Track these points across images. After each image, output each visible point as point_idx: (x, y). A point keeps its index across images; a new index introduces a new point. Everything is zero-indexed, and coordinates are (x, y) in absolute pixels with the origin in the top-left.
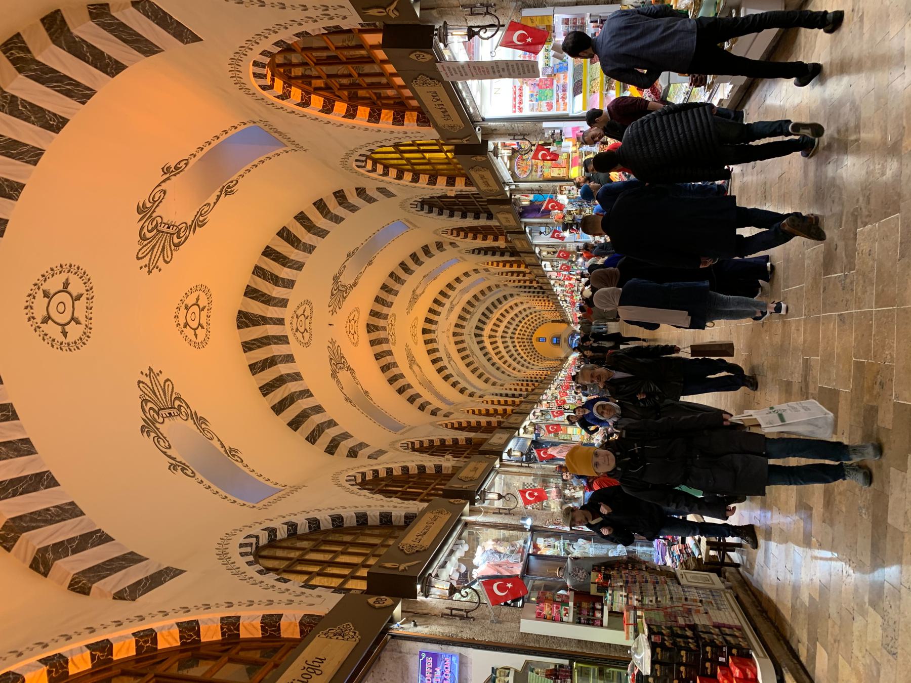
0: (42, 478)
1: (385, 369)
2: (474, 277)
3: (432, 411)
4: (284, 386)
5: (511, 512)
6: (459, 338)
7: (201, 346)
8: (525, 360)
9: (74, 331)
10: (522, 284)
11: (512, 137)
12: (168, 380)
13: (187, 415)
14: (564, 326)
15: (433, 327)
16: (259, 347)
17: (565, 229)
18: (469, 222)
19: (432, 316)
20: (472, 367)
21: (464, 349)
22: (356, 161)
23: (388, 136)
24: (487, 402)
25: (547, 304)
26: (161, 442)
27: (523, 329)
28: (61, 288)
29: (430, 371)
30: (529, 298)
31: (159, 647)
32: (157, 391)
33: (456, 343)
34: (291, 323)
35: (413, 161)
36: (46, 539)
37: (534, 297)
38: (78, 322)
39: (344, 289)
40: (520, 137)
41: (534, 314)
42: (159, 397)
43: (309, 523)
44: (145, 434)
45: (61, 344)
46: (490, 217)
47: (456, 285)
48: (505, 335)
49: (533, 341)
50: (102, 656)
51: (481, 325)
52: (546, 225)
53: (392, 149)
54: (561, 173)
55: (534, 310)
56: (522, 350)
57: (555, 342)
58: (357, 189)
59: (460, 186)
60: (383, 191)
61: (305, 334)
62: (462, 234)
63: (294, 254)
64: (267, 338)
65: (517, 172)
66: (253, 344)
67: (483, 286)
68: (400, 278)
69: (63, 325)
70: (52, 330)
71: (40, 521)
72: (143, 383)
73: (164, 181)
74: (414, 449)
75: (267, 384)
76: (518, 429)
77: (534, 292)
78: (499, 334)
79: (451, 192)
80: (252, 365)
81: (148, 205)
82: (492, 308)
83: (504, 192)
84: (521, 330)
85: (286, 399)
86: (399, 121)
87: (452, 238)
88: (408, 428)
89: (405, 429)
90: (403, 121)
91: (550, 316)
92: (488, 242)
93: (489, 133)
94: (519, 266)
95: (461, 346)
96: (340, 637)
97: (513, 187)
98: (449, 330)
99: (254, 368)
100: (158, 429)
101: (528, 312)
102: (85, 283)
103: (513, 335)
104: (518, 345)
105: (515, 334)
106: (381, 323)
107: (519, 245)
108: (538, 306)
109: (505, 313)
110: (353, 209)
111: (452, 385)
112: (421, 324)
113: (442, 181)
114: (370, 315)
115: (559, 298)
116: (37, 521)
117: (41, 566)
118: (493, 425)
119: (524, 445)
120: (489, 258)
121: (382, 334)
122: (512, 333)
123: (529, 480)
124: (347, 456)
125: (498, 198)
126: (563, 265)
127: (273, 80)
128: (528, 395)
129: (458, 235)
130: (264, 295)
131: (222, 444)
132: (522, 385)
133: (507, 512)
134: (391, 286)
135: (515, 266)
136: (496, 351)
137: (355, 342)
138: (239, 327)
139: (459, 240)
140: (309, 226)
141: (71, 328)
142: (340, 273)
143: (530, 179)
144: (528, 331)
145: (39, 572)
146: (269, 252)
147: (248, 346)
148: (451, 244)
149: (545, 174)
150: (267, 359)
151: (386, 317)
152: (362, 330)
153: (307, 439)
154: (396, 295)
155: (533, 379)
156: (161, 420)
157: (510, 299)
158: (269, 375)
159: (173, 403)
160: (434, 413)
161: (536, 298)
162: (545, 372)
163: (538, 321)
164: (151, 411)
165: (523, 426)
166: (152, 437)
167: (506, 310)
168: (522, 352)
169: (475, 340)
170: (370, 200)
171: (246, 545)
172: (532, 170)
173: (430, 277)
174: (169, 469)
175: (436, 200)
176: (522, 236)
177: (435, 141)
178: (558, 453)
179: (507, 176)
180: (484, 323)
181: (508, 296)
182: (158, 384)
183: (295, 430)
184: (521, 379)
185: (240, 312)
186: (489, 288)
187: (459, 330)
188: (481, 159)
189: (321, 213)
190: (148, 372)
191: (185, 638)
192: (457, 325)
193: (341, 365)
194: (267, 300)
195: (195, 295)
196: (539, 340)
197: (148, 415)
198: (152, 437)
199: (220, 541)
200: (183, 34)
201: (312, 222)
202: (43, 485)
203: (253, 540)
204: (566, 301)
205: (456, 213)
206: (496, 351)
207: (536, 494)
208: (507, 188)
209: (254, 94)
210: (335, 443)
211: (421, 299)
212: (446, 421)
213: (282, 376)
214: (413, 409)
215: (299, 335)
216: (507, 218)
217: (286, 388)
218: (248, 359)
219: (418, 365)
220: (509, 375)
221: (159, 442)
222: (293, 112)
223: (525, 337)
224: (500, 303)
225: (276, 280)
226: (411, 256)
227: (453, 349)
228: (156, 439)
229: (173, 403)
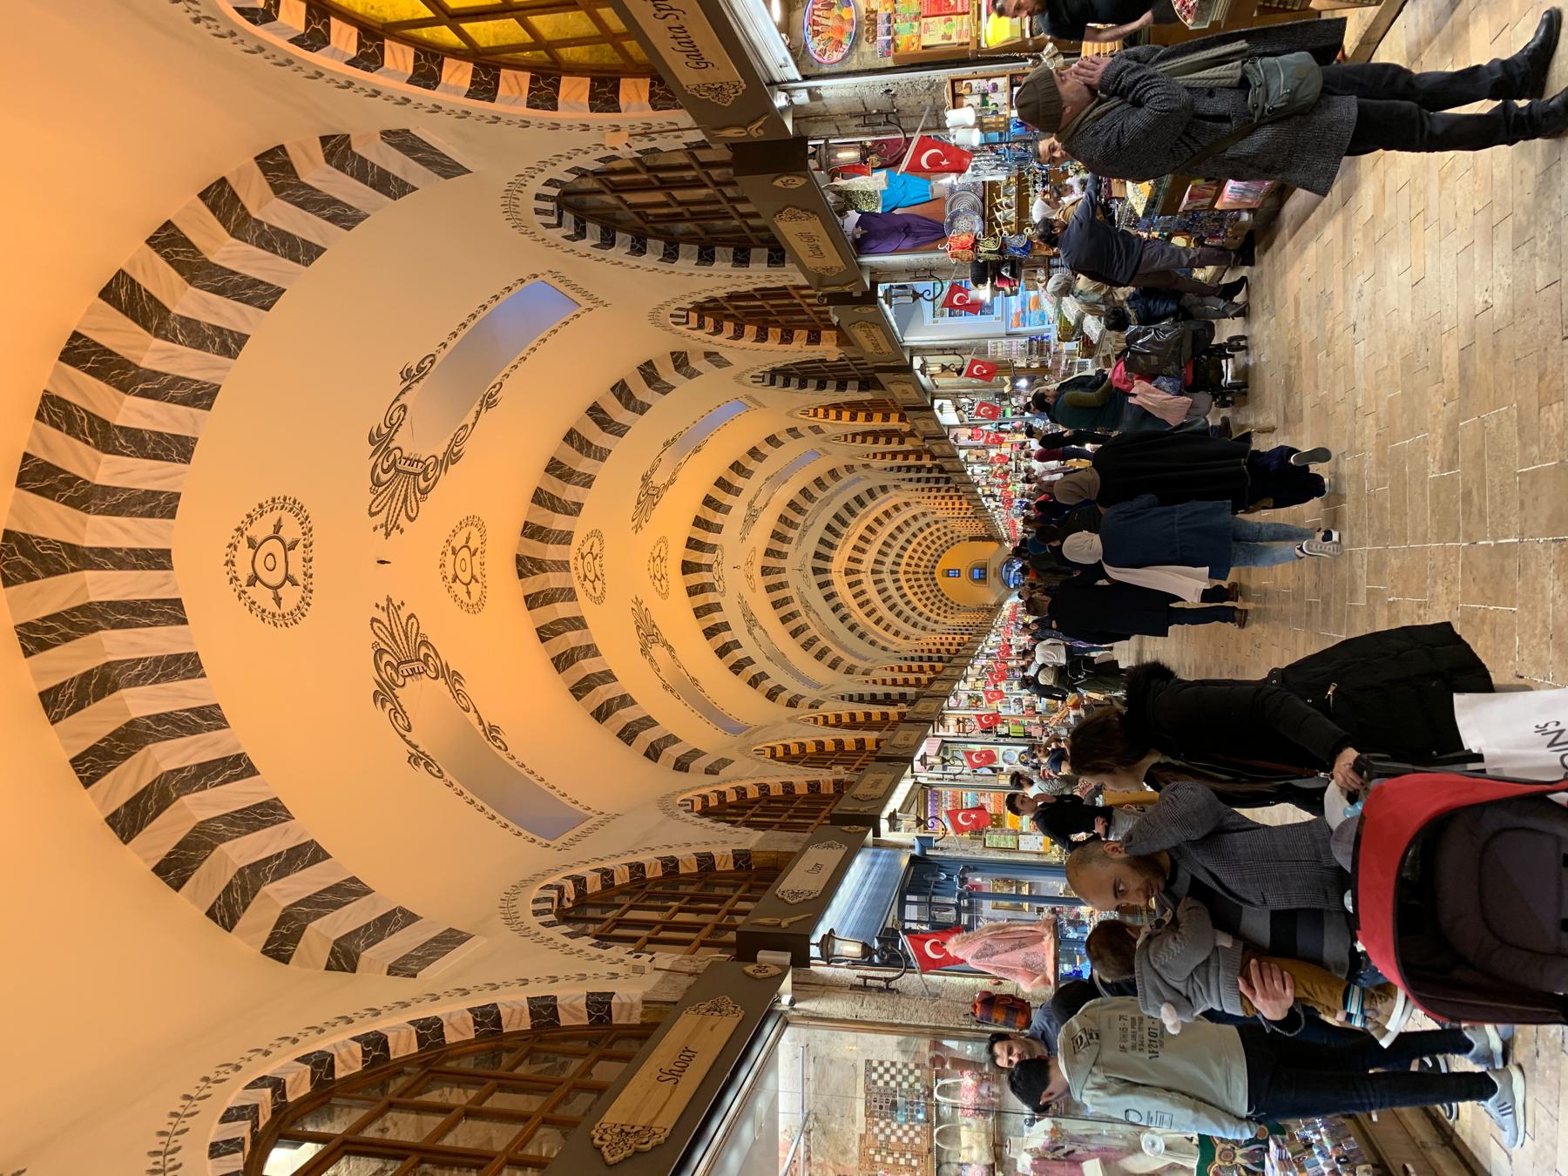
2: (792, 448)
3: (678, 760)
4: (140, 754)
5: (893, 985)
6: (773, 579)
8: (920, 614)
9: (291, 596)
10: (899, 461)
12: (412, 616)
13: (436, 670)
14: (994, 546)
15: (706, 558)
16: (67, 639)
17: (979, 280)
20: (803, 638)
21: (786, 601)
22: (672, 316)
23: (724, 282)
24: (875, 682)
25: (957, 506)
27: (916, 556)
28: (270, 532)
29: (779, 635)
30: (919, 493)
33: (769, 589)
34: (230, 563)
37: (930, 490)
38: (295, 583)
41: (935, 527)
46: (778, 255)
48: (878, 567)
49: (936, 575)
51: (824, 550)
52: (929, 273)
54: (953, 32)
55: (935, 517)
56: (915, 594)
57: (976, 576)
58: (324, 140)
61: (473, 587)
62: (833, 413)
64: (86, 609)
65: (814, 45)
66: (49, 630)
67: (820, 468)
68: (590, 444)
69: (275, 588)
70: (261, 595)
72: (379, 621)
73: (403, 392)
74: (826, 723)
75: (92, 750)
76: (910, 761)
77: (928, 480)
80: (48, 691)
81: (385, 431)
82: (845, 515)
83: (776, 117)
85: (145, 793)
87: (814, 421)
88: (597, 819)
89: (588, 824)
91: (966, 529)
92: (795, 345)
94: (886, 418)
95: (779, 595)
96: (627, 1129)
100: (396, 697)
101: (922, 522)
102: (302, 523)
104: (905, 586)
105: (899, 564)
108: (941, 509)
109: (875, 526)
111: (750, 683)
114: (523, 534)
115: (979, 491)
118: (824, 791)
119: (891, 866)
120: (812, 397)
122: (894, 563)
123: (887, 1047)
124: (328, 968)
126: (982, 405)
127: (560, 216)
128: (950, 660)
130: (71, 480)
132: (921, 669)
133: (883, 984)
134: (569, 464)
135: (878, 417)
136: (861, 599)
141: (287, 591)
143: (854, 65)
144: (925, 558)
148: (708, 355)
149: (902, 41)
150: (88, 675)
151: (565, 538)
152: (757, 571)
155: (935, 656)
157: (881, 497)
160: (792, 704)
161: (934, 493)
162: (957, 637)
163: (944, 539)
165: (885, 814)
166: (387, 710)
167: (877, 520)
168: (914, 599)
169: (814, 580)
170: (692, 374)
171: (547, 900)
173: (684, 444)
178: (979, 956)
179: (774, 54)
180: (832, 546)
181: (877, 492)
183: (177, 889)
184: (909, 654)
186: (833, 474)
187: (773, 562)
188: (868, 310)
189: (224, 222)
190: (384, 604)
192: (769, 553)
195: (591, 540)
196: (947, 573)
197: (384, 675)
198: (387, 710)
199: (504, 897)
200: (447, 168)
201: (196, 251)
203: (554, 894)
204: (993, 496)
205: (683, 248)
206: (861, 599)
207: (973, 816)
208: (780, 101)
209: (197, 20)
211: (668, 496)
212: (814, 713)
213: (132, 723)
214: (756, 698)
215: (588, 584)
217: (145, 761)
218: (37, 675)
219: (665, 644)
220: (884, 649)
222: (350, 84)
223: (920, 570)
224: (862, 504)
226: (613, 389)
227: (761, 604)
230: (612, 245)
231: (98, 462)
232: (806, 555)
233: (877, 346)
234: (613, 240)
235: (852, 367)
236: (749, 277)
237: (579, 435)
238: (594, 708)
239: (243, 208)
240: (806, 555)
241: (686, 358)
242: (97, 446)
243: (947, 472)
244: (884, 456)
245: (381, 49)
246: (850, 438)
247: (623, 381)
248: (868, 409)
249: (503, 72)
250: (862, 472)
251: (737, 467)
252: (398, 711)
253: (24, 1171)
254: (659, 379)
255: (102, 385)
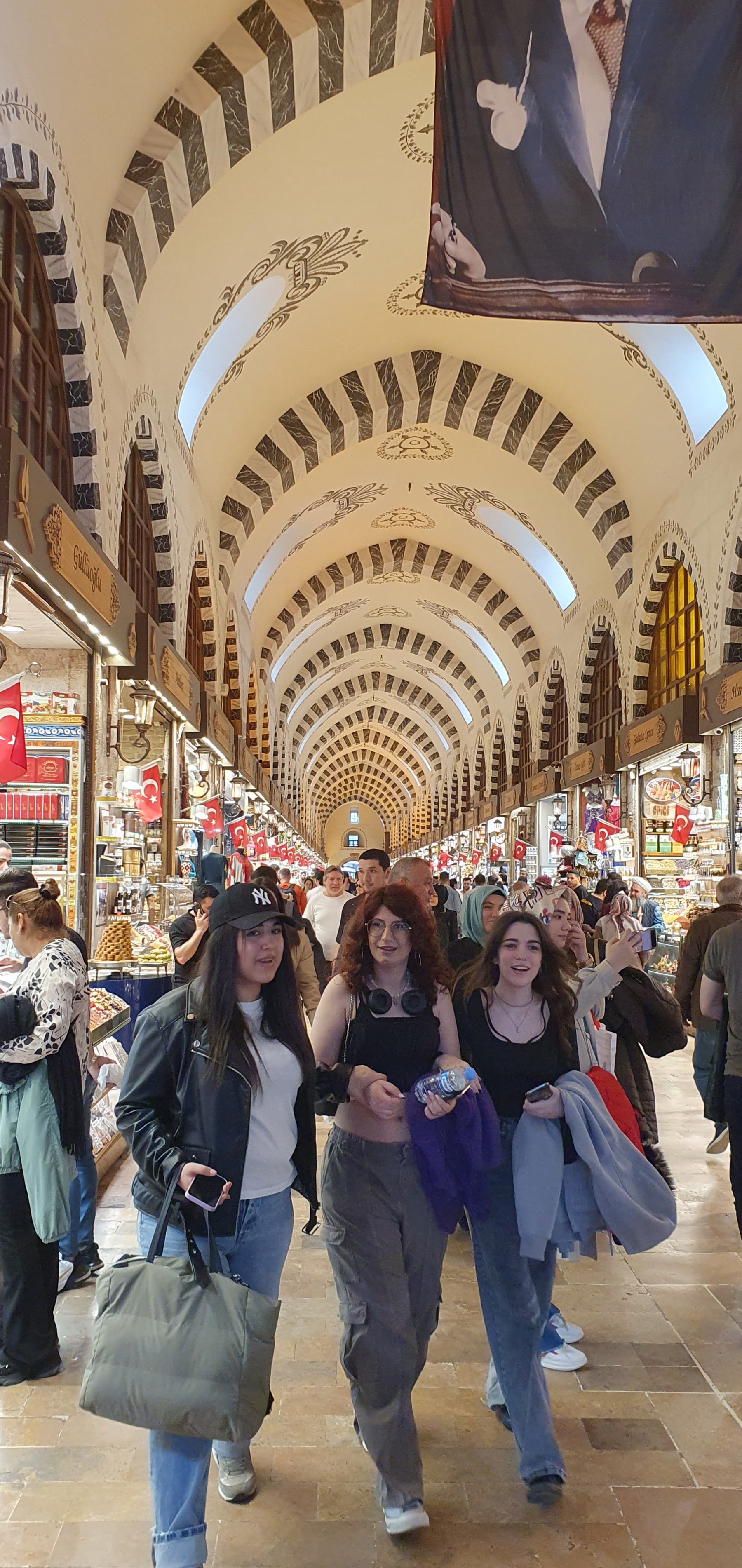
0: (243, 144)
1: (334, 570)
3: (268, 650)
4: (325, 429)
7: (390, 305)
10: (461, 783)
11: (707, 777)
12: (346, 265)
13: (293, 297)
16: (385, 388)
18: (574, 707)
19: (411, 639)
22: (675, 545)
23: (711, 600)
25: (421, 824)
26: (262, 270)
31: (64, 357)
32: (331, 253)
35: (673, 627)
36: (172, 169)
39: (466, 506)
40: (707, 788)
42: (324, 257)
43: (162, 504)
44: (275, 247)
45: (412, 127)
46: (583, 738)
47: (462, 679)
50: (61, 292)
51: (388, 716)
53: (691, 599)
55: (410, 804)
58: (630, 538)
59: (632, 697)
60: (627, 579)
63: (530, 440)
64: (400, 399)
65: (655, 782)
68: (480, 592)
71: (193, 154)
72: (345, 235)
78: (370, 746)
79: (626, 684)
84: (373, 781)
86: (732, 619)
87: (545, 676)
90: (732, 625)
93: (713, 746)
97: (632, 776)
98: (384, 665)
99: (351, 380)
100: (279, 263)
103: (365, 768)
106: (408, 563)
107: (536, 781)
110: (600, 531)
111: (298, 676)
112: (398, 623)
113: (642, 670)
114: (421, 544)
116: (194, 150)
117: (140, 168)
121: (389, 563)
124: (221, 533)
125: (617, 754)
129: (551, 686)
131: (250, 350)
137: (379, 523)
138: (414, 354)
139: (542, 686)
140: (575, 462)
142: (493, 502)
145: (131, 166)
146: (532, 399)
147: (385, 369)
150: (366, 400)
151: (416, 569)
152: (397, 533)
153: (245, 468)
154: (452, 585)
156: (291, 264)
158: (342, 404)
159: (313, 276)
164: (305, 250)
169: (363, 708)
170: (612, 558)
172: (657, 802)
174: (227, 288)
175: (611, 656)
176: (552, 787)
177: (702, 664)
179: (649, 767)
182: (341, 254)
185: (439, 355)
187: (383, 681)
188: (677, 732)
189: (594, 483)
191: (74, 388)
192: (391, 678)
193: (345, 505)
194: (459, 398)
197: (300, 247)
201: (579, 468)
202: (234, 148)
210: (241, 513)
216: (583, 766)
221: (263, 267)
225: (490, 411)
228: (268, 263)
229: (313, 276)
230: (590, 648)
231: (475, 409)
232: (385, 702)
233: (535, 788)
234: (593, 649)
235: (560, 744)
236: (716, 626)
237: (487, 584)
238: (303, 593)
239: (600, 494)
240: (385, 702)
241: (535, 660)
242: (483, 408)
243: (452, 820)
244: (466, 772)
245: (659, 590)
246: (481, 750)
247: (522, 616)
248: (499, 768)
249: (651, 638)
250: (454, 753)
251: (461, 668)
252: (268, 267)
253: (125, 351)
254: (522, 640)
255: (515, 413)
